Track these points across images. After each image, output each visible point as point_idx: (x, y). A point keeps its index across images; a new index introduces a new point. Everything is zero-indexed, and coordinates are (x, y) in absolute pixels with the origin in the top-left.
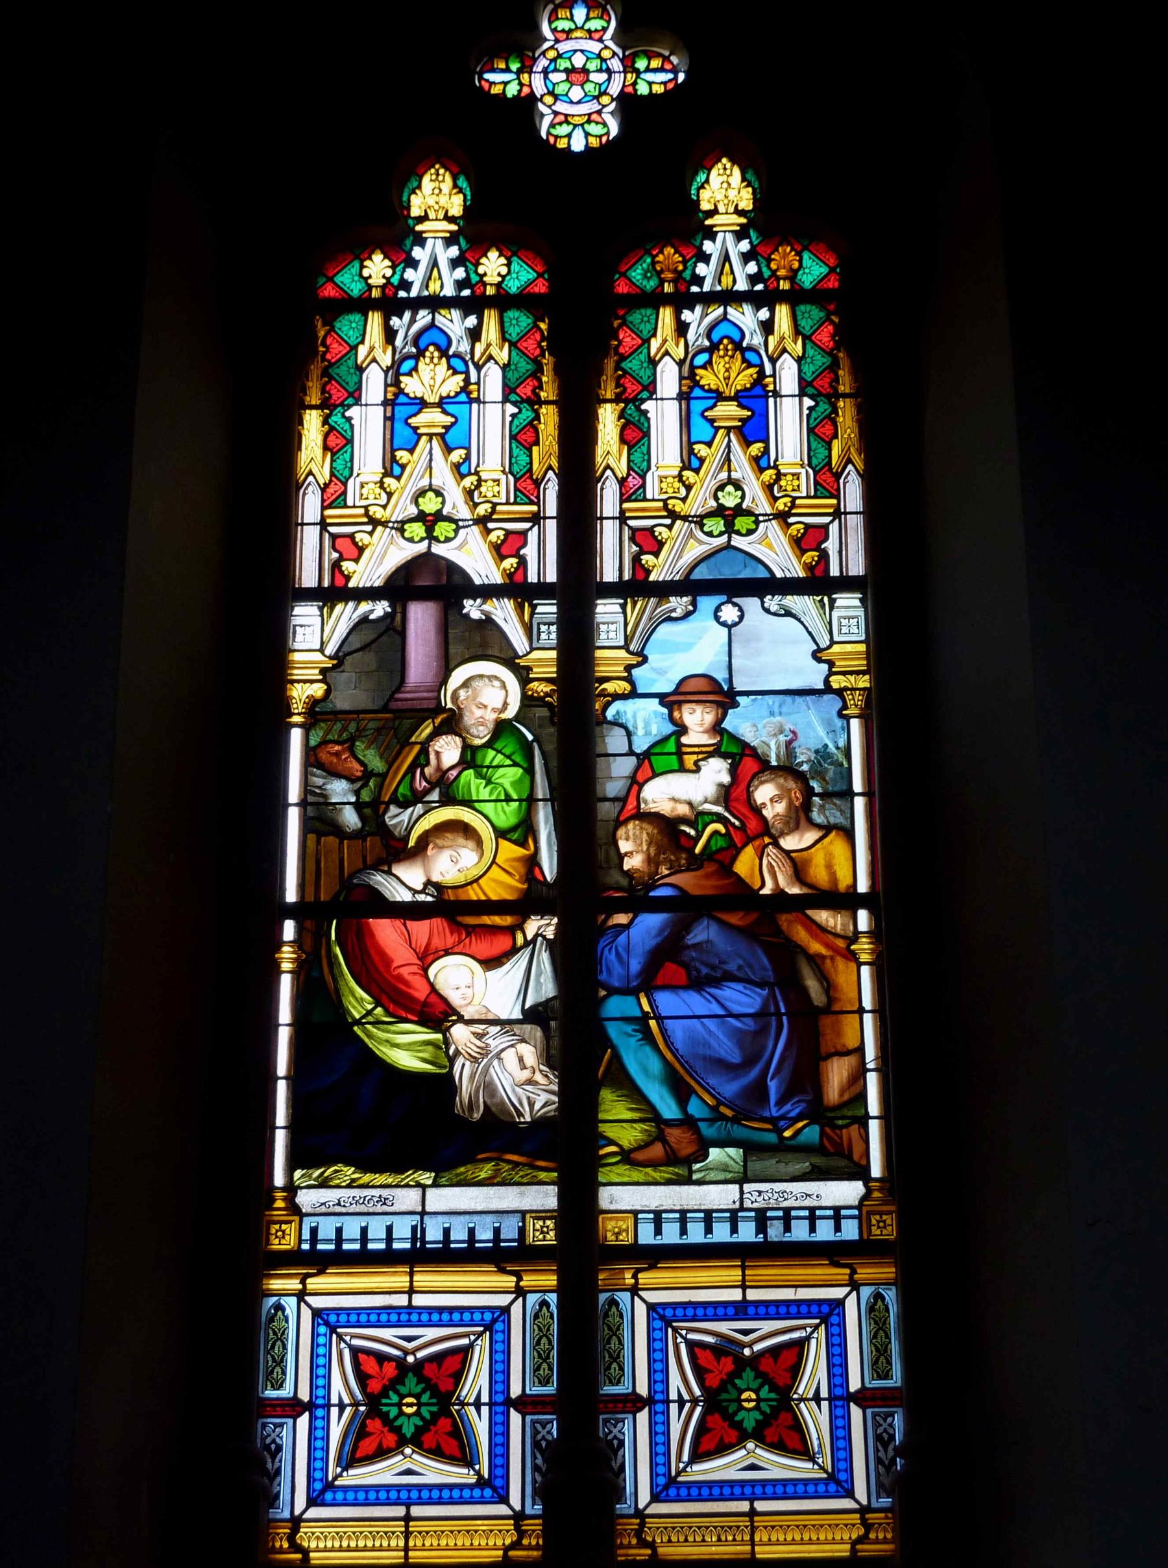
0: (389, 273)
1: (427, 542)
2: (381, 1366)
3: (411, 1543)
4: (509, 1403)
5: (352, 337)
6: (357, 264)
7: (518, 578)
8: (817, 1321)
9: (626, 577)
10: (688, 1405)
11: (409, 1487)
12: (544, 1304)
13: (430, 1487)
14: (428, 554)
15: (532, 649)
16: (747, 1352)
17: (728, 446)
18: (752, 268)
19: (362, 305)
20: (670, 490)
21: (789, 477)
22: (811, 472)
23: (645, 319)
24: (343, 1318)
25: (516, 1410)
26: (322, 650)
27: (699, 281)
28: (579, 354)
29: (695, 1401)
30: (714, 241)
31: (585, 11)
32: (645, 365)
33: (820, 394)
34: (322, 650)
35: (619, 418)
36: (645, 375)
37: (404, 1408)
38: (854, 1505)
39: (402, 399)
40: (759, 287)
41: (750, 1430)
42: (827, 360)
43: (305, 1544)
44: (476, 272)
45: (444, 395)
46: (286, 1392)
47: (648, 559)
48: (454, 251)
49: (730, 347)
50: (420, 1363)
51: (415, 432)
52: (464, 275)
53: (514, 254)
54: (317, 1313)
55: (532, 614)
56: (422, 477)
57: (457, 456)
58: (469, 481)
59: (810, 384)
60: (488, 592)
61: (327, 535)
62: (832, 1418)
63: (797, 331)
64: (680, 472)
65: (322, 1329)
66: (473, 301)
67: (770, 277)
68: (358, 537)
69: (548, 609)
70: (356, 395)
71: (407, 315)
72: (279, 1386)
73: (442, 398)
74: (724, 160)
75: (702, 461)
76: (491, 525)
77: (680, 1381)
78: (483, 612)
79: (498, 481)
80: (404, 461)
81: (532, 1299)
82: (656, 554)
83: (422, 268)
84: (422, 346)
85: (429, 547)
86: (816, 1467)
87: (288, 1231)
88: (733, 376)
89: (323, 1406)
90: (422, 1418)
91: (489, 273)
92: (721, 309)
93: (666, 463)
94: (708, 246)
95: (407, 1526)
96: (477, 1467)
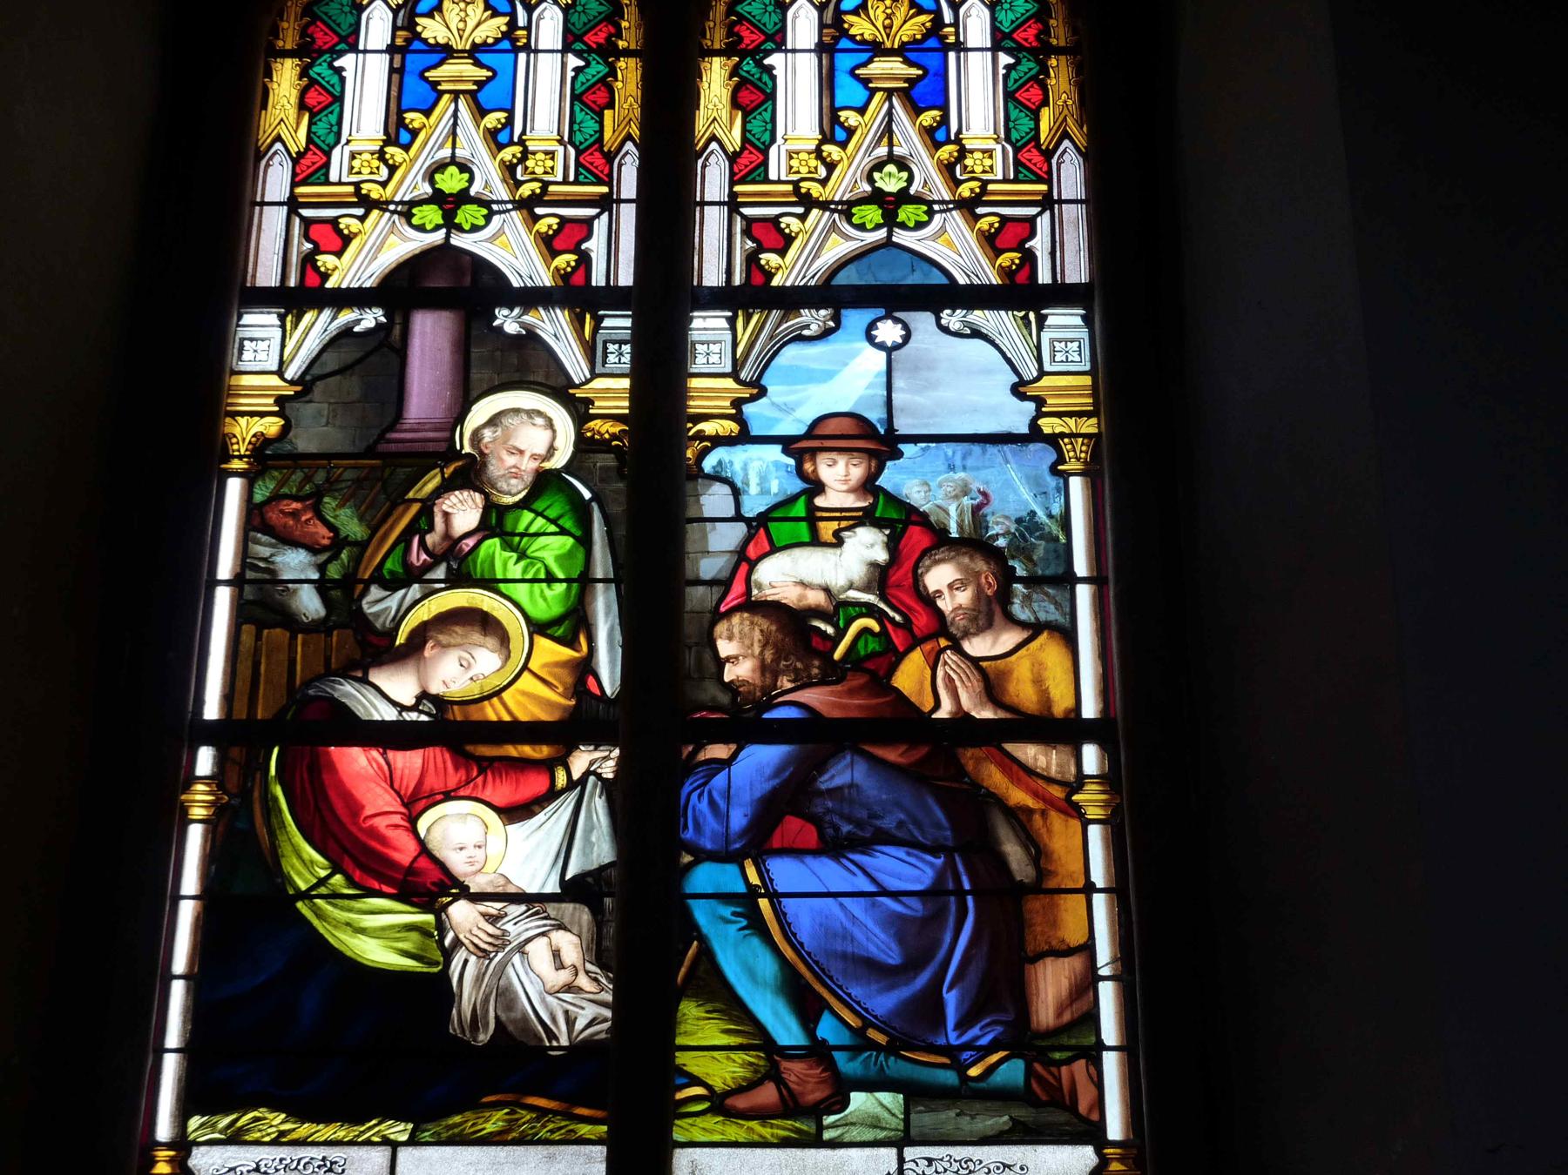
9: (737, 280)
14: (446, 245)
17: (455, 115)
20: (804, 170)
21: (540, 156)
22: (1009, 148)
26: (280, 373)
34: (280, 373)
36: (770, 22)
45: (478, 41)
47: (769, 259)
51: (867, 88)
55: (596, 328)
56: (441, 147)
57: (492, 120)
58: (947, 152)
59: (1009, 36)
60: (532, 298)
61: (297, 220)
64: (382, 148)
68: (343, 222)
69: (619, 322)
70: (778, 38)
75: (851, 132)
80: (416, 125)
82: (782, 253)
93: (797, 133)
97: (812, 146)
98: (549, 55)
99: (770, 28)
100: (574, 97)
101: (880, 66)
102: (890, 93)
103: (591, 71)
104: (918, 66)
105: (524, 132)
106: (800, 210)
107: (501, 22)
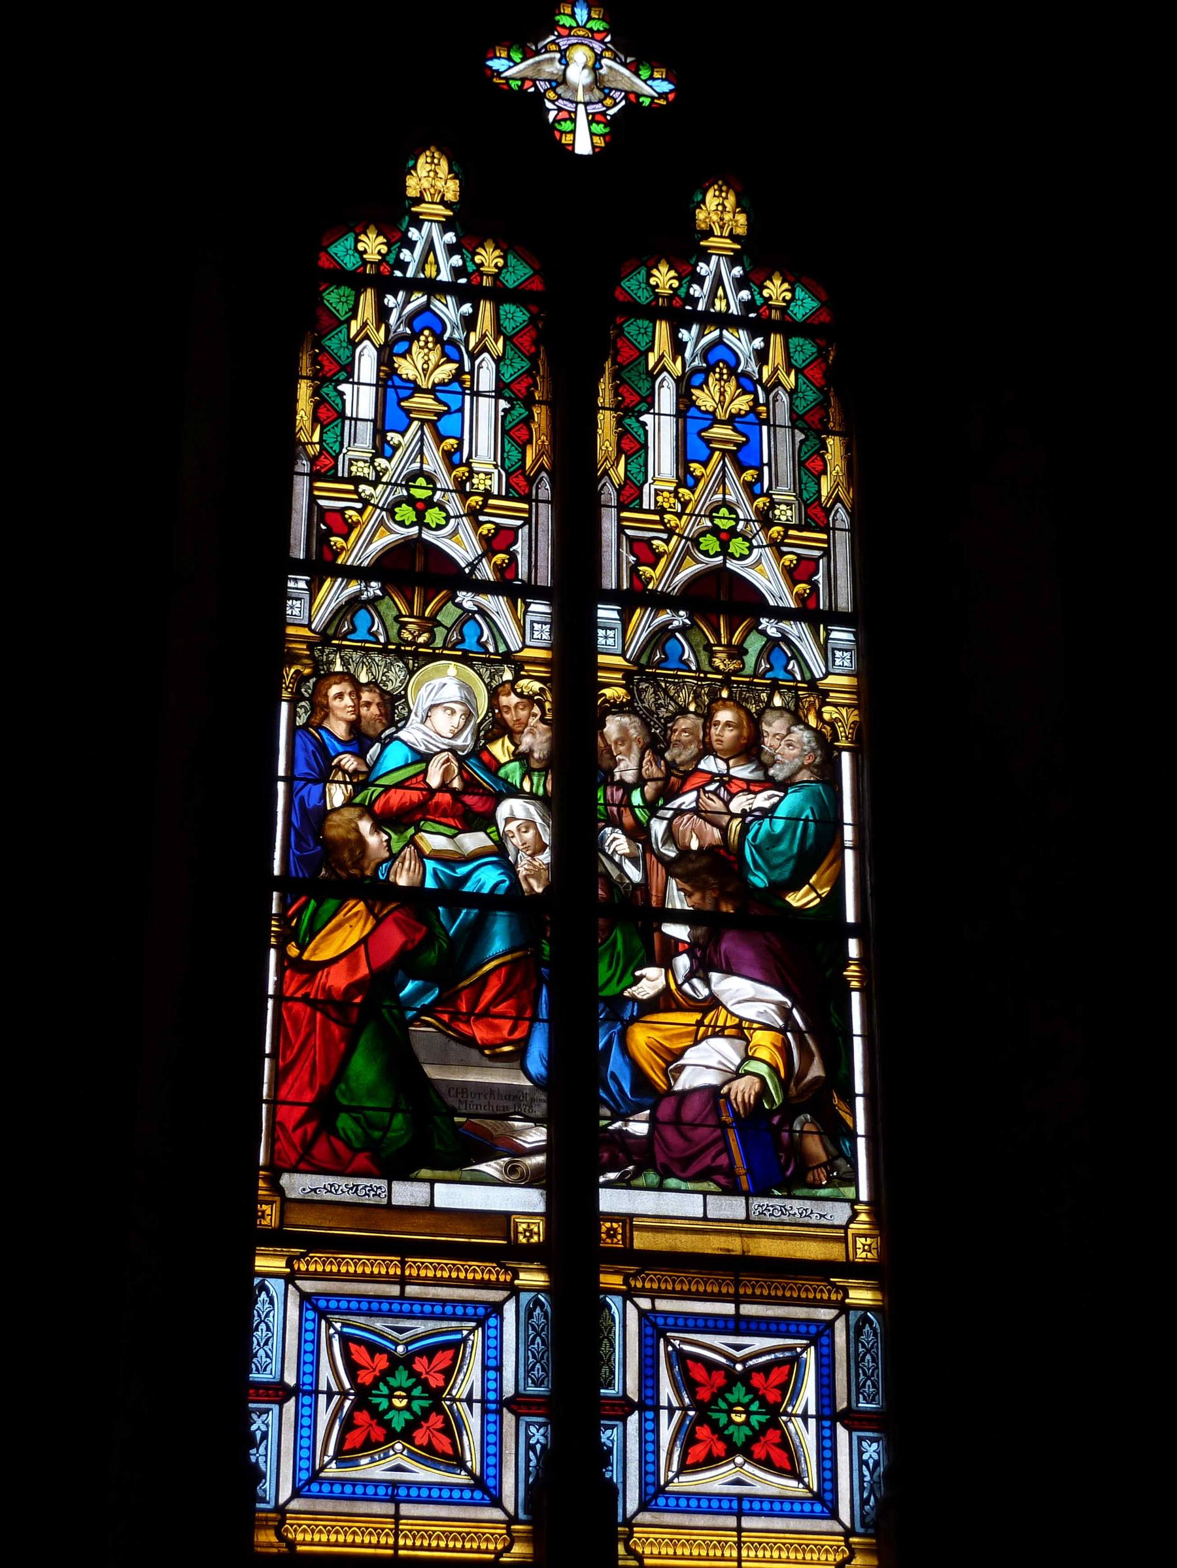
0: (384, 249)
1: (721, 558)
2: (710, 1374)
3: (744, 1553)
4: (641, 1407)
5: (342, 311)
6: (643, 272)
7: (811, 605)
8: (473, 1324)
10: (336, 1398)
11: (740, 1497)
12: (537, 1303)
13: (761, 1498)
14: (722, 568)
15: (525, 646)
16: (400, 1349)
18: (457, 260)
19: (653, 312)
23: (642, 331)
24: (671, 1321)
25: (510, 1411)
26: (309, 626)
27: (404, 266)
28: (573, 360)
29: (344, 1394)
30: (420, 230)
31: (585, 12)
32: (344, 344)
33: (810, 428)
34: (623, 655)
35: (313, 396)
36: (344, 354)
37: (733, 1415)
38: (839, 1529)
39: (693, 412)
40: (463, 281)
41: (739, 1444)
42: (526, 365)
43: (639, 1550)
44: (473, 260)
45: (436, 381)
46: (614, 1391)
47: (645, 570)
48: (737, 271)
49: (725, 371)
50: (748, 1372)
51: (408, 417)
52: (460, 263)
53: (798, 280)
54: (305, 1297)
55: (526, 612)
56: (414, 461)
57: (450, 443)
59: (801, 417)
60: (781, 614)
62: (820, 1438)
63: (499, 330)
64: (676, 488)
65: (310, 1315)
66: (467, 289)
67: (762, 305)
70: (649, 399)
71: (695, 328)
72: (610, 1385)
73: (434, 385)
74: (433, 148)
75: (697, 480)
76: (482, 518)
77: (330, 1372)
78: (779, 630)
79: (490, 474)
80: (697, 473)
81: (525, 1297)
83: (708, 283)
84: (417, 328)
85: (725, 562)
86: (801, 1486)
87: (268, 1212)
88: (728, 399)
89: (309, 1393)
90: (752, 1428)
91: (369, 251)
92: (717, 333)
94: (702, 268)
95: (739, 1537)
96: (806, 1480)
97: (671, 487)
98: (368, 387)
99: (344, 361)
100: (504, 432)
101: (718, 431)
102: (423, 422)
103: (515, 413)
104: (743, 435)
105: (470, 456)
106: (359, 505)
107: (452, 367)
